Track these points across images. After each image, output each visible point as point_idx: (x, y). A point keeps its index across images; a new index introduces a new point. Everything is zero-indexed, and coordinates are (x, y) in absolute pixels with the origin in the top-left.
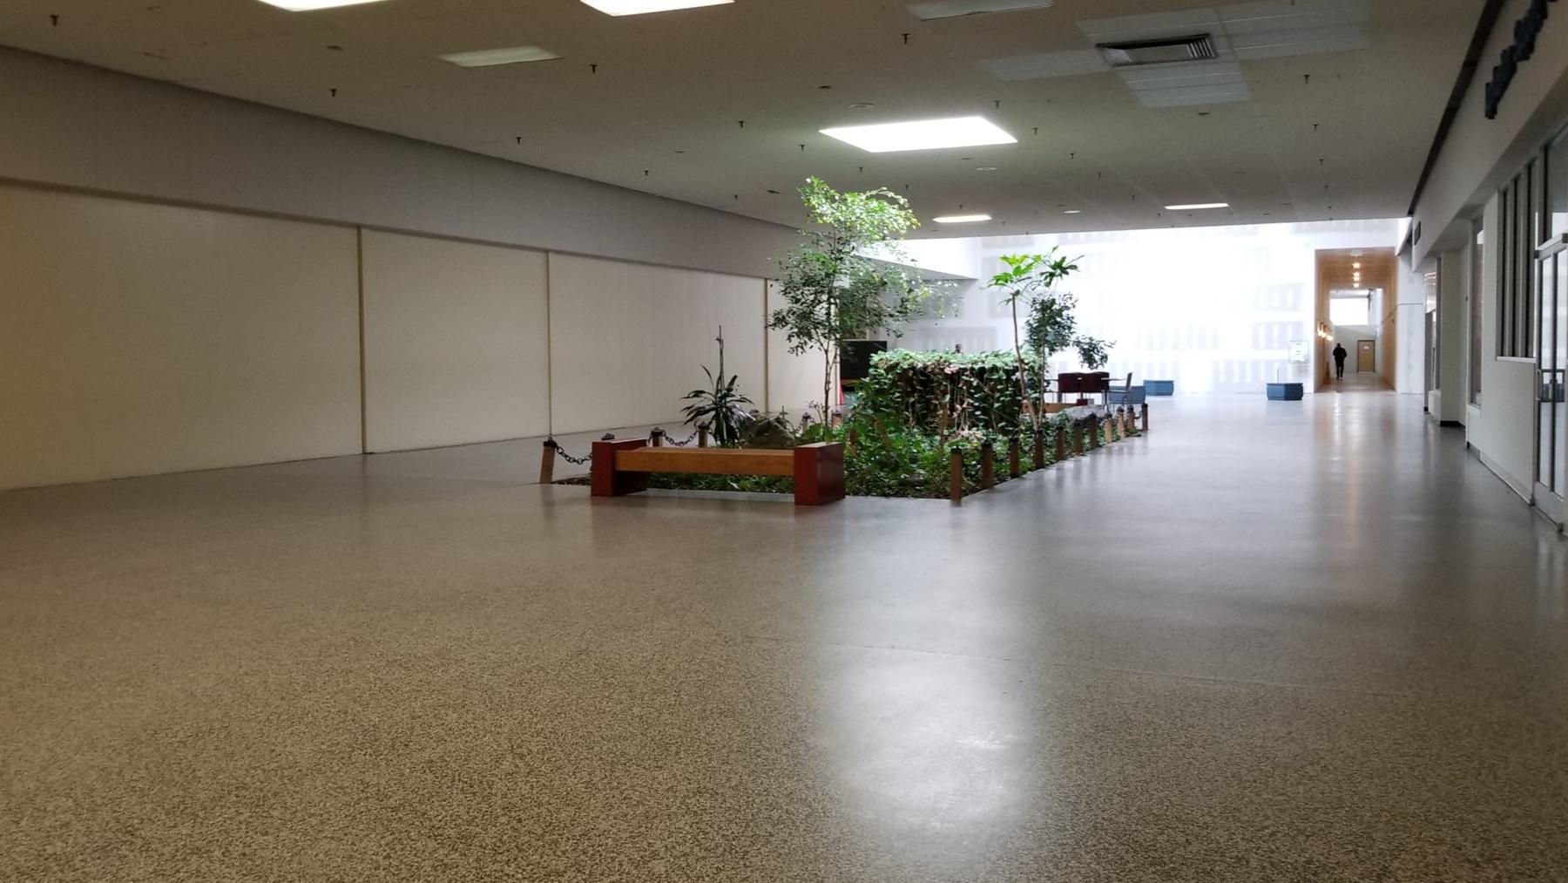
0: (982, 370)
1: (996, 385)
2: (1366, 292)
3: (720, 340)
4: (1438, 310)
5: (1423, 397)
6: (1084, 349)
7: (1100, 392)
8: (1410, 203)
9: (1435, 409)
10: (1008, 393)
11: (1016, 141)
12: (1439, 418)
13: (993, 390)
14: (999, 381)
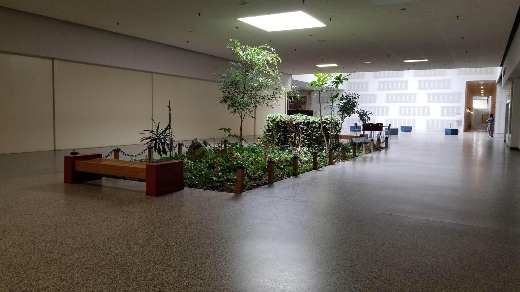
0: (308, 123)
1: (314, 129)
2: (486, 98)
3: (169, 107)
4: (511, 102)
5: (504, 135)
6: (361, 115)
7: (378, 131)
8: (501, 60)
9: (508, 141)
10: (319, 132)
11: (326, 26)
12: (510, 145)
13: (313, 131)
14: (316, 127)
